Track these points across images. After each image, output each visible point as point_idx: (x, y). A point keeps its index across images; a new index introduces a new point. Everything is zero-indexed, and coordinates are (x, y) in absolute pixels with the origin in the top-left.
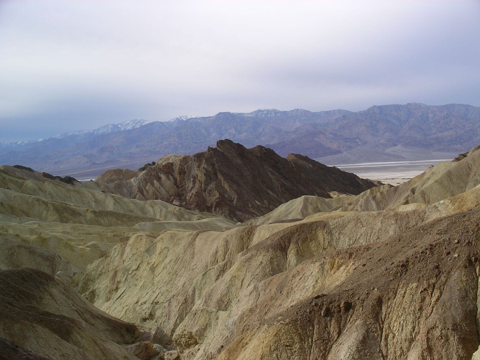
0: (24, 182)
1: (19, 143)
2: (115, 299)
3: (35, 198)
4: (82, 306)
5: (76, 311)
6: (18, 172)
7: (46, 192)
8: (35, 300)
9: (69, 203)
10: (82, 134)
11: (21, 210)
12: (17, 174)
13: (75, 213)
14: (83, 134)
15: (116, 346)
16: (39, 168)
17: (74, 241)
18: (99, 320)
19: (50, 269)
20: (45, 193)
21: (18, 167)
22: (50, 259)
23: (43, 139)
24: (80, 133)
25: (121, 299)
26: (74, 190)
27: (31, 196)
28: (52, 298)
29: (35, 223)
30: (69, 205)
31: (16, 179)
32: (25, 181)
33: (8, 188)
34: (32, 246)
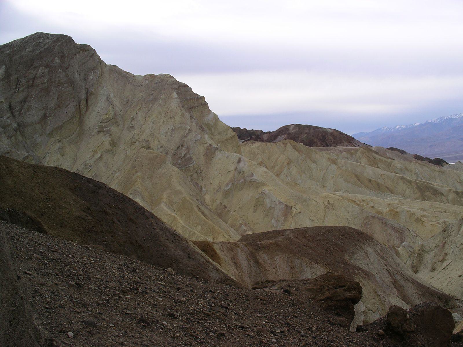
0: (392, 161)
1: (397, 127)
2: (439, 270)
3: (400, 176)
4: (395, 268)
5: (388, 271)
6: (388, 153)
7: (412, 171)
8: (348, 254)
9: (433, 183)
10: (458, 117)
11: (386, 187)
12: (388, 154)
13: (436, 193)
14: (459, 117)
15: (399, 301)
16: (411, 150)
17: (428, 217)
18: (410, 283)
19: (399, 241)
20: (411, 173)
21: (392, 149)
22: (400, 231)
23: (419, 124)
24: (456, 117)
25: (445, 270)
26: (439, 170)
27: (397, 174)
28: (366, 256)
29: (396, 199)
30: (431, 184)
31: (386, 159)
32: (393, 161)
33: (378, 167)
34: (385, 218)
